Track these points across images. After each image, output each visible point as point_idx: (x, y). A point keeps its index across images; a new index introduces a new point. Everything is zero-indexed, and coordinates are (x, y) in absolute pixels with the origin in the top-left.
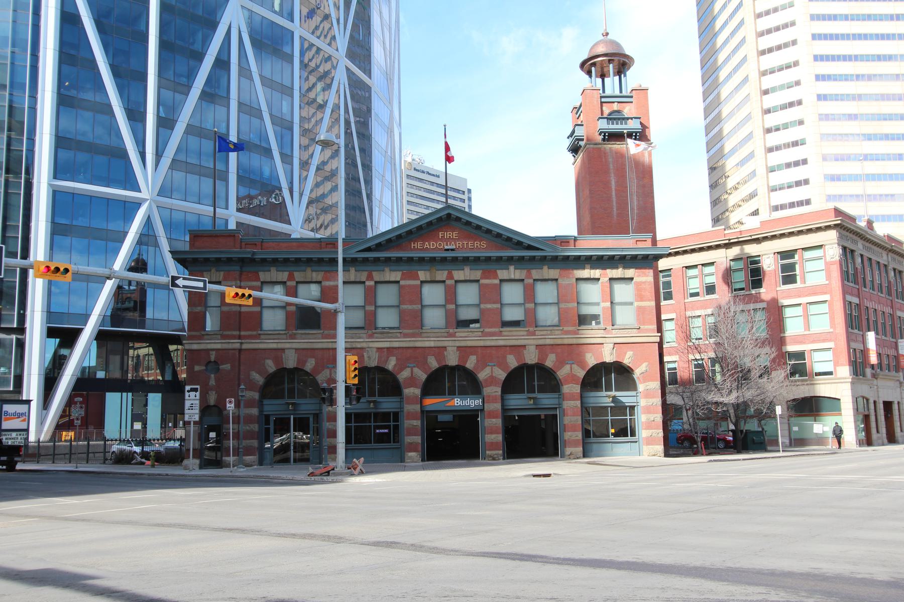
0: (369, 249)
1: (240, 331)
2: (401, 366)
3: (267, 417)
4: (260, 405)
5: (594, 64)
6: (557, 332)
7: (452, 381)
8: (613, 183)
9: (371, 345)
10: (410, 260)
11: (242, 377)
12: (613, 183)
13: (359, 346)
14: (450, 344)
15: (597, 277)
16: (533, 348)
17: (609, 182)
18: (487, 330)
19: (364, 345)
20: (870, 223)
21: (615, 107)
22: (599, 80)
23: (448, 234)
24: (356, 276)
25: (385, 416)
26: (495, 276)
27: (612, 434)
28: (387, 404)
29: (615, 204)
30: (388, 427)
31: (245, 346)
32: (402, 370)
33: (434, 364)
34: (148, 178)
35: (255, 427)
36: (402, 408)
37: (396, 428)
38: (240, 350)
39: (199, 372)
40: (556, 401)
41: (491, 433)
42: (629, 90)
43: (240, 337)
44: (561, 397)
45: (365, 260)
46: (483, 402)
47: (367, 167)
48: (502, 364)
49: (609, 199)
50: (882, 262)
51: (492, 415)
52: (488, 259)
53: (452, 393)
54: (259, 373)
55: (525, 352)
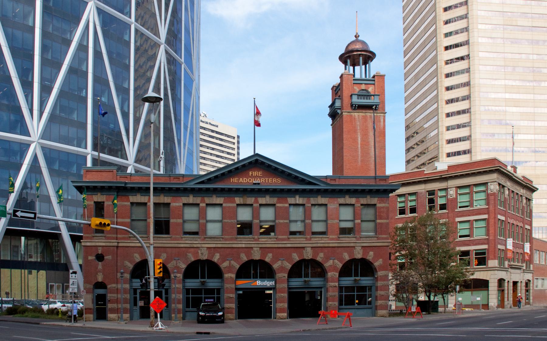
0: (202, 182)
1: (117, 234)
2: (327, 259)
3: (135, 290)
4: (131, 282)
5: (349, 57)
6: (325, 239)
7: (255, 270)
8: (359, 139)
9: (203, 245)
10: (230, 190)
11: (119, 264)
12: (359, 139)
13: (195, 246)
14: (256, 245)
15: (353, 203)
16: (309, 249)
17: (357, 138)
18: (280, 237)
19: (199, 245)
20: (515, 168)
21: (363, 87)
22: (351, 68)
23: (255, 173)
24: (193, 200)
25: (210, 291)
26: (286, 202)
27: (357, 303)
28: (212, 284)
29: (359, 153)
30: (213, 298)
31: (120, 245)
32: (224, 261)
33: (245, 259)
34: (36, 125)
35: (128, 296)
36: (223, 286)
37: (219, 299)
38: (117, 247)
39: (92, 260)
40: (322, 283)
41: (281, 303)
42: (372, 76)
43: (117, 239)
44: (326, 280)
45: (200, 190)
46: (276, 283)
47: (178, 121)
48: (289, 259)
49: (356, 151)
50: (520, 194)
51: (282, 291)
52: (282, 191)
53: (255, 277)
54: (130, 262)
55: (304, 251)
